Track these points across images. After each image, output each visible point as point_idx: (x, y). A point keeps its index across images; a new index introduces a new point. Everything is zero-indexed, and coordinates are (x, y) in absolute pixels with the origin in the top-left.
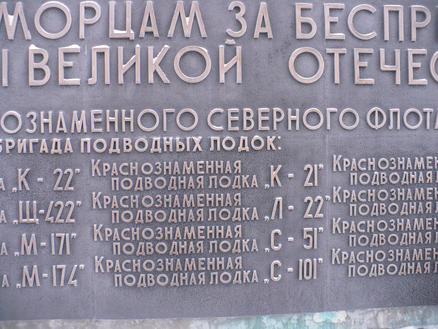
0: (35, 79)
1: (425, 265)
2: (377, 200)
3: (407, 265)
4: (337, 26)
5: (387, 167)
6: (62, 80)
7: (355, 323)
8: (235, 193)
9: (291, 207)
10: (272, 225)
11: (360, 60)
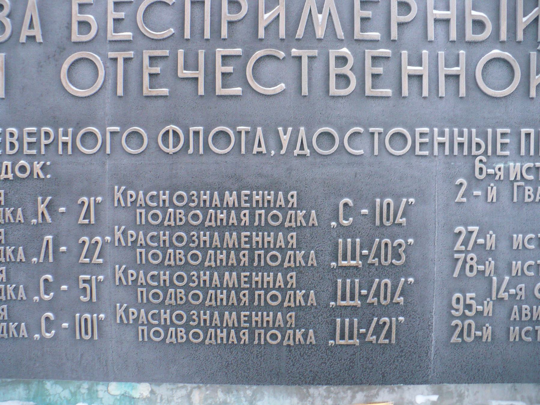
0: (337, 88)
1: (241, 333)
2: (172, 245)
3: (216, 332)
4: (124, 23)
5: (184, 203)
6: (369, 91)
7: (161, 399)
8: (289, 233)
9: (63, 249)
10: (41, 268)
11: (151, 65)
